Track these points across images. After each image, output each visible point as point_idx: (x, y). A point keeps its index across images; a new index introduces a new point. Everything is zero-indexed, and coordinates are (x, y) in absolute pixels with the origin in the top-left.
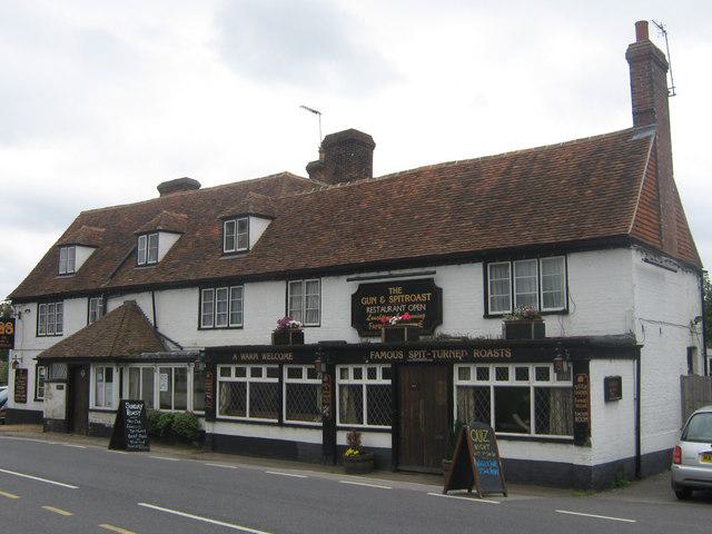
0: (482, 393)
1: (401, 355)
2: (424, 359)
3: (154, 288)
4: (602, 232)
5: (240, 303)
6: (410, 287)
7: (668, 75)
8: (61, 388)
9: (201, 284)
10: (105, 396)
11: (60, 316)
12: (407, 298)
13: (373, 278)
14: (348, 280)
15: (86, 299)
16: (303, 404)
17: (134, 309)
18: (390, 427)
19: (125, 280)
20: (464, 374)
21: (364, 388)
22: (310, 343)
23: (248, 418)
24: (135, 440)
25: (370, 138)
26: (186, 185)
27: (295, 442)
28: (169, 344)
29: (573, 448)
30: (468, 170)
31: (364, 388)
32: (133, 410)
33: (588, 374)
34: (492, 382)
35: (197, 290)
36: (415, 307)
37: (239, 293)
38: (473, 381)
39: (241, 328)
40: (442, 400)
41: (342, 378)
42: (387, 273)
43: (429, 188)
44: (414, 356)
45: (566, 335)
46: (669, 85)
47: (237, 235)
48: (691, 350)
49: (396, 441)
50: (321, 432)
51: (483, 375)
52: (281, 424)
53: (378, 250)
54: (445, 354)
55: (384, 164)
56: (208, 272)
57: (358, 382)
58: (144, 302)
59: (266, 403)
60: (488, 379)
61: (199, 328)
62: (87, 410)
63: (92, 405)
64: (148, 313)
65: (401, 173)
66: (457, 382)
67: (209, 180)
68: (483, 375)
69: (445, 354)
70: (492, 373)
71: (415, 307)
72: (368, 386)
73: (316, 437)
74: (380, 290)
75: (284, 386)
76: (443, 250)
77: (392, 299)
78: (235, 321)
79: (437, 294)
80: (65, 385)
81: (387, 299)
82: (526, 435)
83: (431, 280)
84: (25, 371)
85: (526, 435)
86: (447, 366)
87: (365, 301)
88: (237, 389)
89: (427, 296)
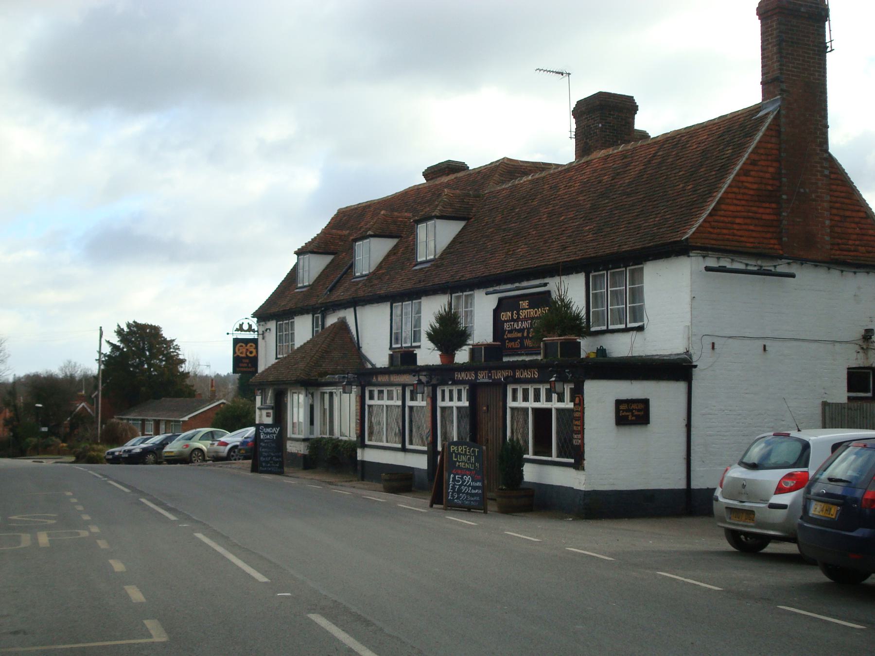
0: (542, 415)
2: (486, 380)
3: (355, 303)
5: (471, 311)
7: (827, 23)
11: (637, 295)
13: (511, 290)
14: (487, 294)
15: (389, 304)
17: (342, 325)
18: (572, 461)
19: (340, 294)
21: (530, 411)
22: (422, 364)
24: (267, 462)
25: (631, 99)
26: (451, 168)
27: (413, 468)
29: (571, 472)
30: (625, 157)
31: (530, 411)
32: (268, 433)
33: (583, 396)
35: (389, 304)
37: (637, 277)
41: (412, 399)
42: (509, 286)
45: (636, 354)
46: (828, 39)
50: (682, 485)
52: (404, 449)
55: (654, 121)
56: (395, 287)
57: (547, 405)
58: (348, 315)
60: (619, 403)
67: (475, 161)
75: (508, 411)
76: (370, 292)
77: (523, 314)
81: (518, 314)
82: (549, 459)
85: (549, 459)
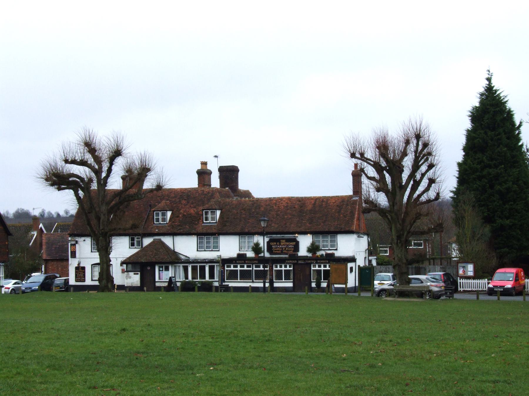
1: (296, 262)
4: (347, 229)
6: (288, 240)
8: (138, 274)
9: (198, 234)
10: (162, 277)
12: (287, 243)
16: (261, 275)
20: (314, 266)
23: (239, 281)
28: (181, 256)
34: (322, 268)
36: (291, 246)
38: (317, 268)
39: (219, 251)
40: (308, 273)
43: (287, 206)
44: (300, 262)
47: (209, 216)
48: (365, 258)
49: (294, 285)
51: (320, 266)
52: (253, 282)
53: (274, 227)
54: (309, 262)
59: (246, 275)
61: (197, 251)
62: (155, 282)
63: (157, 279)
64: (171, 246)
65: (274, 198)
66: (312, 268)
68: (320, 266)
69: (309, 262)
70: (322, 266)
71: (291, 246)
72: (324, 270)
73: (261, 285)
74: (278, 241)
77: (282, 244)
78: (216, 248)
79: (297, 243)
80: (139, 273)
83: (295, 239)
84: (84, 268)
86: (310, 264)
87: (272, 244)
88: (319, 272)
89: (294, 243)
